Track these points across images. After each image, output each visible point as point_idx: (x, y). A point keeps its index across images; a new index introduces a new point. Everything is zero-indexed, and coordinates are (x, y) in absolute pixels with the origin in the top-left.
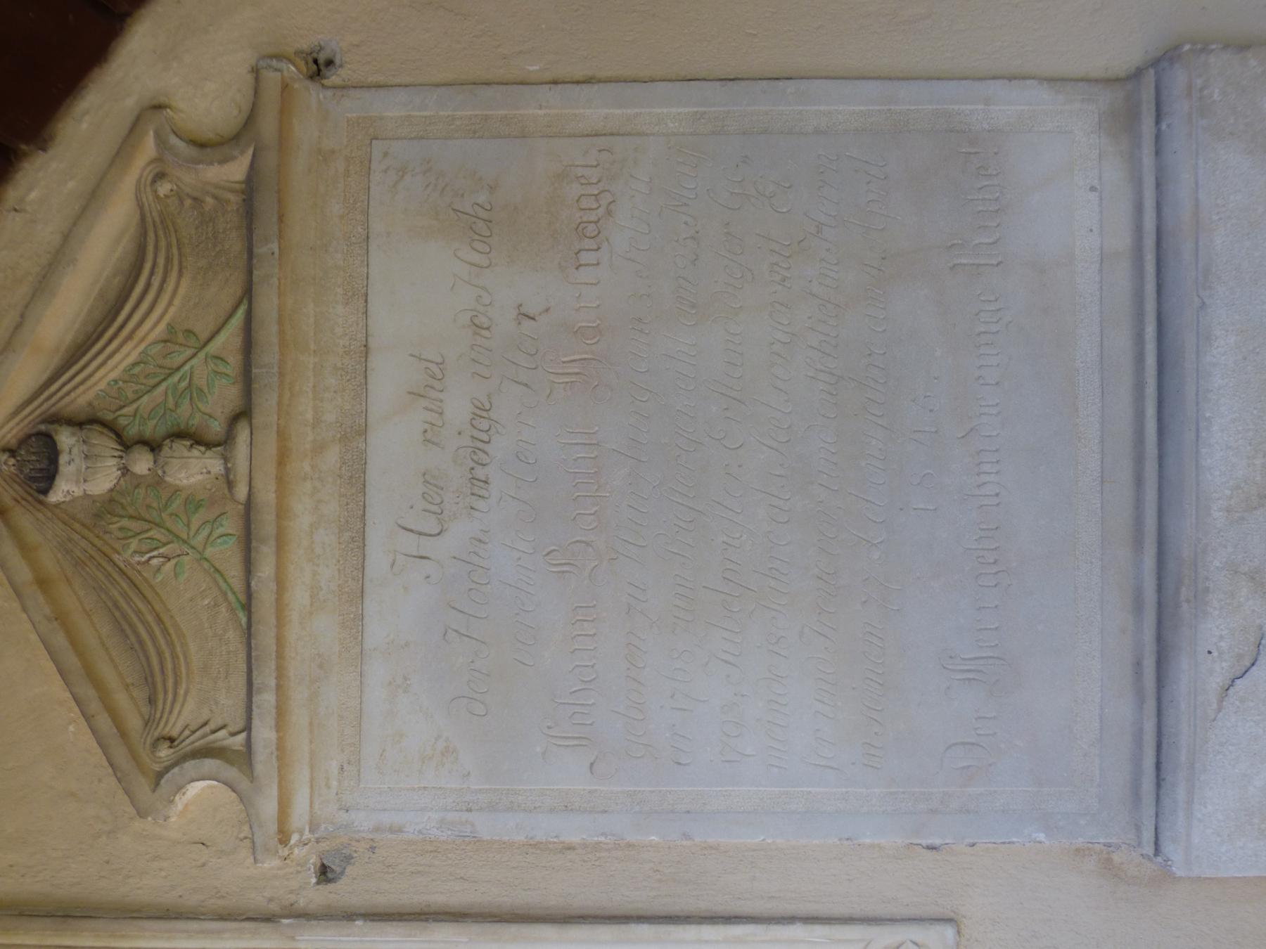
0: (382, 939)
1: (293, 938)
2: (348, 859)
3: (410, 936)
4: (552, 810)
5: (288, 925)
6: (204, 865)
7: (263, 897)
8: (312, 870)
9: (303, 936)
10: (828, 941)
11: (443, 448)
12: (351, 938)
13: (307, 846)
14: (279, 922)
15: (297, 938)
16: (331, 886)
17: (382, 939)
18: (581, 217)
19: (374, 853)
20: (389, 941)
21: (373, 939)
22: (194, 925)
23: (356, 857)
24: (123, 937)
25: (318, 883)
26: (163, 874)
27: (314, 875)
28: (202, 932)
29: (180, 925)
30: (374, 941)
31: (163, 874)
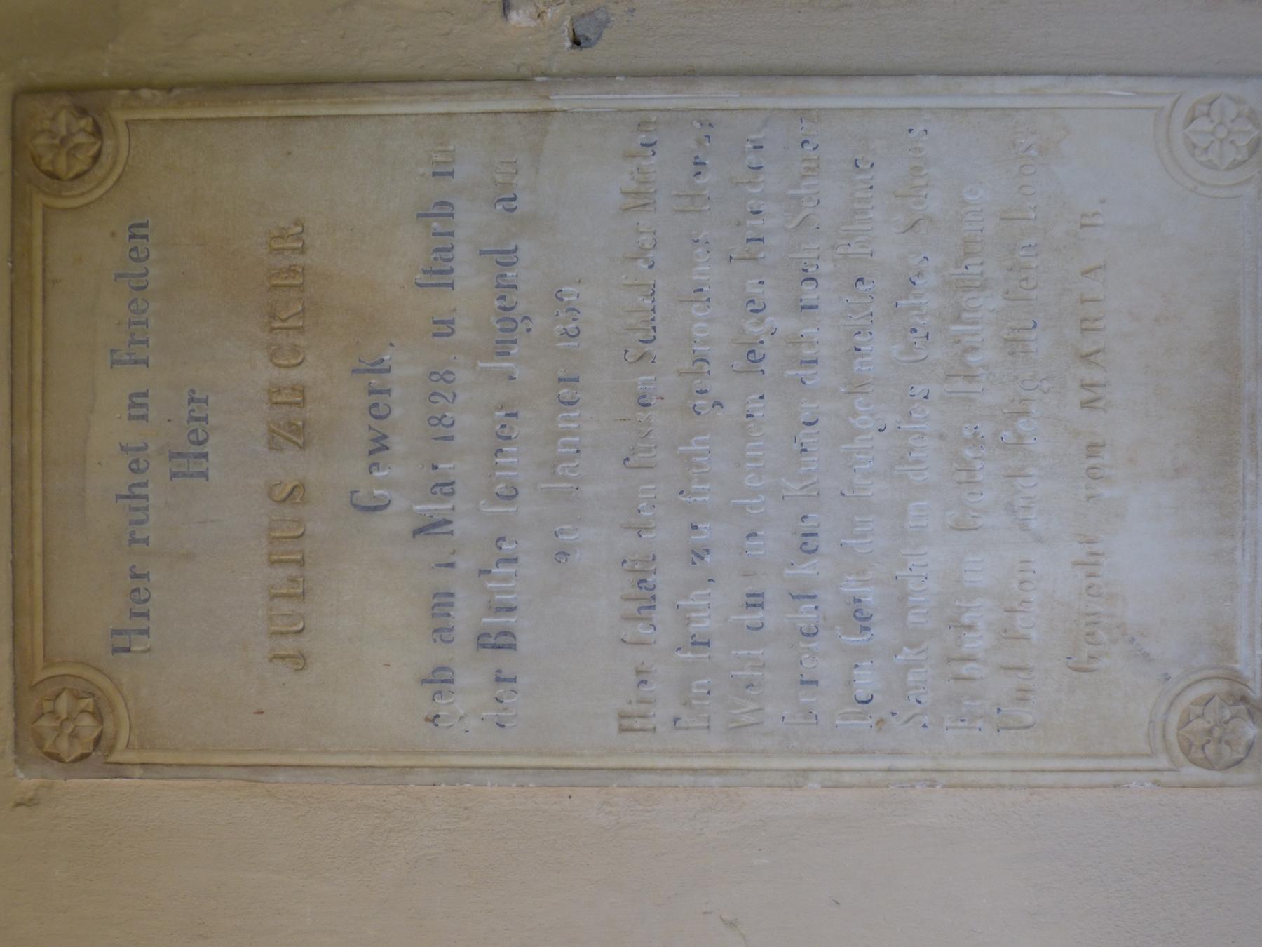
0: (647, 96)
1: (547, 98)
2: (605, 24)
3: (675, 92)
4: (889, 754)
5: (543, 83)
6: (448, 34)
7: (513, 63)
8: (566, 33)
9: (558, 95)
10: (1134, 95)
11: (482, 253)
12: (611, 96)
13: (561, 6)
14: (534, 80)
15: (551, 97)
16: (586, 52)
17: (647, 96)
18: (702, 829)
19: (632, 16)
20: (653, 98)
21: (635, 96)
22: (440, 87)
23: (614, 21)
24: (360, 102)
25: (572, 48)
26: (403, 44)
27: (567, 38)
28: (448, 93)
29: (423, 87)
30: (637, 99)
31: (403, 44)
